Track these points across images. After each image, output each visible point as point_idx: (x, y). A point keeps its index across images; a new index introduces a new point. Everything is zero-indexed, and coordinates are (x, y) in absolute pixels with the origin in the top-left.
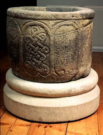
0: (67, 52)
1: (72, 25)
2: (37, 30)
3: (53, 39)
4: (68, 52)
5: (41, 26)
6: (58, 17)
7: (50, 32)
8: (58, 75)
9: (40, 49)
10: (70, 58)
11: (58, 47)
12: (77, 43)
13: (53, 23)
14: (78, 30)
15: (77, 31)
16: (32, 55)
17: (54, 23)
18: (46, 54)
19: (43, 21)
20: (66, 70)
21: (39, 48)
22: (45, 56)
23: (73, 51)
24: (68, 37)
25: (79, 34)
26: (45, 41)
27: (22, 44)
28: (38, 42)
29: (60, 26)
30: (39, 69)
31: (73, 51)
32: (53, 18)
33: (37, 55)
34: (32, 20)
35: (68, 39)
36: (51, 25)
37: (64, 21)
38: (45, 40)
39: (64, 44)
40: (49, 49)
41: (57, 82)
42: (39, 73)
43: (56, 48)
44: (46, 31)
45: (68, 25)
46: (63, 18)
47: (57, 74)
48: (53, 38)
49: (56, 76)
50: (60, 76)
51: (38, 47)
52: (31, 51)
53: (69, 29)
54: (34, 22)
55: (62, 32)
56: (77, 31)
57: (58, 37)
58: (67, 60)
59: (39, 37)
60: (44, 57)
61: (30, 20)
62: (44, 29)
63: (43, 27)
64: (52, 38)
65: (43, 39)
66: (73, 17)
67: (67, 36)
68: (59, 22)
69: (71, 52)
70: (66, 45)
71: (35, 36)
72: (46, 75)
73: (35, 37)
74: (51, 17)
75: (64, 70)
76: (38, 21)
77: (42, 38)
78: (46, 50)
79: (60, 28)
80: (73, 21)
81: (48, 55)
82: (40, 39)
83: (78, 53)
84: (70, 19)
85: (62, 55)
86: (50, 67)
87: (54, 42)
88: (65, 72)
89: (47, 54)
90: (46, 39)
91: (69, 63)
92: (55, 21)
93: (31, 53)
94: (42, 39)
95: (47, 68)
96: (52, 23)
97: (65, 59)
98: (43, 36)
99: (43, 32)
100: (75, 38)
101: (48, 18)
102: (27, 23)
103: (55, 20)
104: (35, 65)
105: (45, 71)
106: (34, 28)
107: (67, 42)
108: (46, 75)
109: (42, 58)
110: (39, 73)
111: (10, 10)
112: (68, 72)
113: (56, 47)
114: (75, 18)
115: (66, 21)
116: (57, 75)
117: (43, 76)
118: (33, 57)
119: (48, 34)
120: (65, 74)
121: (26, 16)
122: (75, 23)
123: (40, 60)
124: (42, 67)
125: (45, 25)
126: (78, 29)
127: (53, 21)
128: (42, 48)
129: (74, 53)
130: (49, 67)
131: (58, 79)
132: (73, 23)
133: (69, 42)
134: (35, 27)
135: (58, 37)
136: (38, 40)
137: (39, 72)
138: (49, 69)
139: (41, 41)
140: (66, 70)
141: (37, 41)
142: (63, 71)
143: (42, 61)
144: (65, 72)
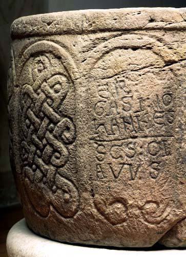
0: (130, 140)
1: (150, 48)
2: (44, 68)
3: (83, 95)
4: (136, 137)
5: (54, 54)
6: (100, 24)
7: (77, 71)
8: (106, 218)
9: (52, 125)
10: (144, 159)
11: (101, 119)
12: (170, 111)
13: (87, 43)
14: (174, 66)
15: (171, 70)
16: (35, 149)
17: (90, 42)
18: (67, 143)
19: (58, 38)
20: (130, 202)
21: (49, 124)
22: (65, 150)
23: (156, 136)
24: (134, 89)
25: (179, 78)
26: (62, 100)
27: (16, 115)
28: (45, 104)
29: (107, 52)
30: (50, 193)
31: (156, 136)
32: (86, 25)
33: (45, 146)
34: (36, 38)
35: (135, 95)
36: (80, 50)
37: (120, 35)
38: (64, 97)
39: (120, 110)
40: (75, 126)
41: (107, 243)
42: (51, 208)
43: (93, 122)
44: (65, 68)
45: (135, 48)
46: (117, 25)
47: (102, 213)
48: (84, 89)
49: (98, 220)
50: (114, 224)
51: (47, 121)
52: (32, 134)
53: (136, 62)
54: (38, 45)
55: (111, 72)
56: (171, 70)
57: (100, 88)
58: (130, 165)
59: (48, 88)
60: (60, 154)
61: (32, 39)
62: (62, 63)
63: (59, 58)
64: (81, 90)
65: (59, 94)
66: (152, 21)
67: (128, 82)
68: (104, 39)
69: (149, 139)
70: (126, 114)
71: (40, 87)
72: (72, 217)
73: (39, 91)
74: (79, 24)
75: (123, 201)
76: (48, 40)
77: (56, 92)
78: (68, 129)
79: (107, 57)
80: (152, 33)
81: (71, 147)
82: (49, 93)
83: (177, 145)
84: (140, 29)
85: (114, 148)
86: (80, 187)
87: (88, 104)
88: (127, 208)
89: (71, 143)
90: (66, 95)
91: (140, 178)
92: (93, 36)
93: (32, 142)
94: (56, 95)
95: (70, 191)
96: (83, 41)
97: (124, 164)
98: (57, 86)
99: (60, 74)
100: (160, 94)
101: (72, 27)
102: (25, 47)
103: (94, 32)
104: (41, 180)
105: (67, 201)
106: (39, 62)
107: (128, 103)
108: (72, 217)
109: (58, 158)
110: (54, 207)
111: (24, 21)
112: (137, 212)
113: (95, 120)
114: (161, 24)
115: (125, 34)
116: (102, 218)
117: (63, 218)
118: (35, 153)
119: (70, 76)
120: (127, 214)
121: (25, 27)
122: (160, 40)
123: (51, 164)
124: (58, 188)
125: (62, 51)
126: (175, 62)
127: (85, 37)
128: (55, 124)
129: (159, 143)
130: (77, 188)
131: (108, 234)
132: (152, 40)
133: (136, 106)
134: (41, 58)
135: (100, 88)
136: (48, 97)
137: (51, 203)
138: (76, 194)
139: (53, 100)
140: (130, 202)
141: (43, 102)
142: (120, 205)
143: (58, 167)
144: (127, 208)
